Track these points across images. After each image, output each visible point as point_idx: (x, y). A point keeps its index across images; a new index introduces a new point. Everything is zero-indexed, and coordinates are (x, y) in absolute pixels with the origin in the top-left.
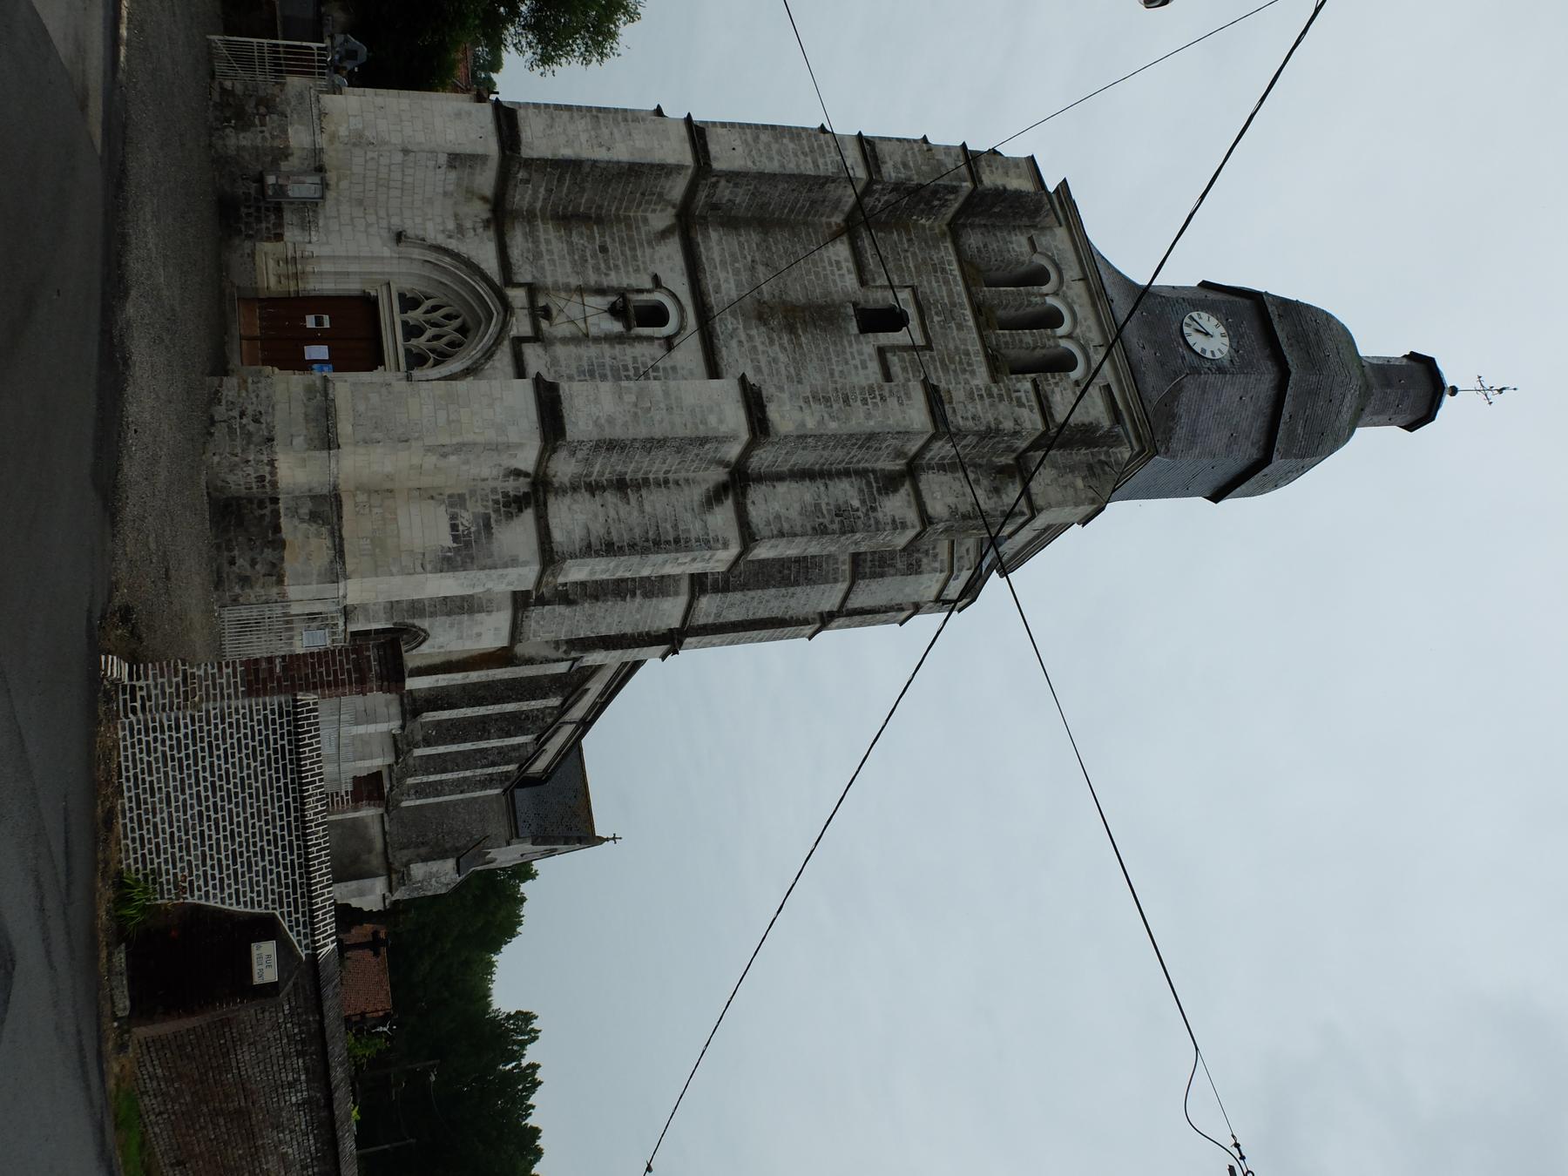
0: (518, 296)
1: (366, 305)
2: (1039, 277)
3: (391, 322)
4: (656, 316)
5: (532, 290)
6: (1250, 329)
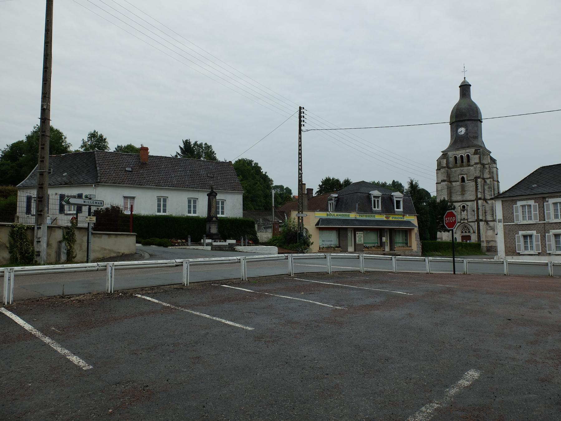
0: (462, 221)
1: (462, 236)
2: (456, 158)
3: (464, 234)
4: (464, 207)
5: (461, 220)
6: (460, 124)
